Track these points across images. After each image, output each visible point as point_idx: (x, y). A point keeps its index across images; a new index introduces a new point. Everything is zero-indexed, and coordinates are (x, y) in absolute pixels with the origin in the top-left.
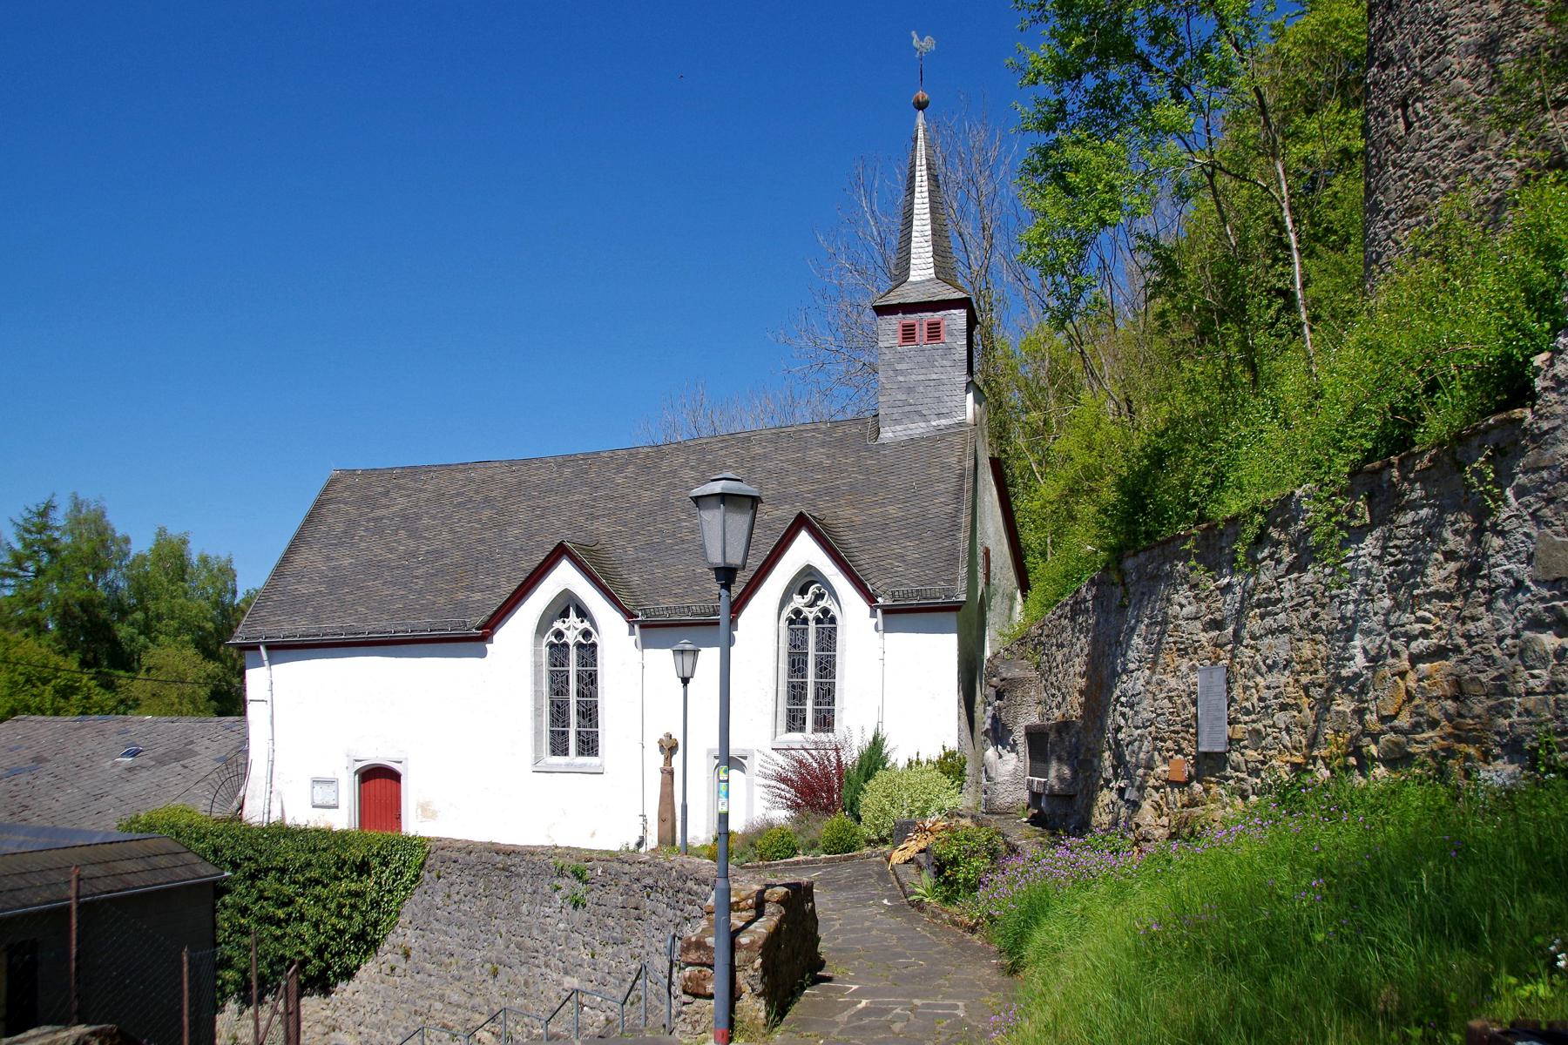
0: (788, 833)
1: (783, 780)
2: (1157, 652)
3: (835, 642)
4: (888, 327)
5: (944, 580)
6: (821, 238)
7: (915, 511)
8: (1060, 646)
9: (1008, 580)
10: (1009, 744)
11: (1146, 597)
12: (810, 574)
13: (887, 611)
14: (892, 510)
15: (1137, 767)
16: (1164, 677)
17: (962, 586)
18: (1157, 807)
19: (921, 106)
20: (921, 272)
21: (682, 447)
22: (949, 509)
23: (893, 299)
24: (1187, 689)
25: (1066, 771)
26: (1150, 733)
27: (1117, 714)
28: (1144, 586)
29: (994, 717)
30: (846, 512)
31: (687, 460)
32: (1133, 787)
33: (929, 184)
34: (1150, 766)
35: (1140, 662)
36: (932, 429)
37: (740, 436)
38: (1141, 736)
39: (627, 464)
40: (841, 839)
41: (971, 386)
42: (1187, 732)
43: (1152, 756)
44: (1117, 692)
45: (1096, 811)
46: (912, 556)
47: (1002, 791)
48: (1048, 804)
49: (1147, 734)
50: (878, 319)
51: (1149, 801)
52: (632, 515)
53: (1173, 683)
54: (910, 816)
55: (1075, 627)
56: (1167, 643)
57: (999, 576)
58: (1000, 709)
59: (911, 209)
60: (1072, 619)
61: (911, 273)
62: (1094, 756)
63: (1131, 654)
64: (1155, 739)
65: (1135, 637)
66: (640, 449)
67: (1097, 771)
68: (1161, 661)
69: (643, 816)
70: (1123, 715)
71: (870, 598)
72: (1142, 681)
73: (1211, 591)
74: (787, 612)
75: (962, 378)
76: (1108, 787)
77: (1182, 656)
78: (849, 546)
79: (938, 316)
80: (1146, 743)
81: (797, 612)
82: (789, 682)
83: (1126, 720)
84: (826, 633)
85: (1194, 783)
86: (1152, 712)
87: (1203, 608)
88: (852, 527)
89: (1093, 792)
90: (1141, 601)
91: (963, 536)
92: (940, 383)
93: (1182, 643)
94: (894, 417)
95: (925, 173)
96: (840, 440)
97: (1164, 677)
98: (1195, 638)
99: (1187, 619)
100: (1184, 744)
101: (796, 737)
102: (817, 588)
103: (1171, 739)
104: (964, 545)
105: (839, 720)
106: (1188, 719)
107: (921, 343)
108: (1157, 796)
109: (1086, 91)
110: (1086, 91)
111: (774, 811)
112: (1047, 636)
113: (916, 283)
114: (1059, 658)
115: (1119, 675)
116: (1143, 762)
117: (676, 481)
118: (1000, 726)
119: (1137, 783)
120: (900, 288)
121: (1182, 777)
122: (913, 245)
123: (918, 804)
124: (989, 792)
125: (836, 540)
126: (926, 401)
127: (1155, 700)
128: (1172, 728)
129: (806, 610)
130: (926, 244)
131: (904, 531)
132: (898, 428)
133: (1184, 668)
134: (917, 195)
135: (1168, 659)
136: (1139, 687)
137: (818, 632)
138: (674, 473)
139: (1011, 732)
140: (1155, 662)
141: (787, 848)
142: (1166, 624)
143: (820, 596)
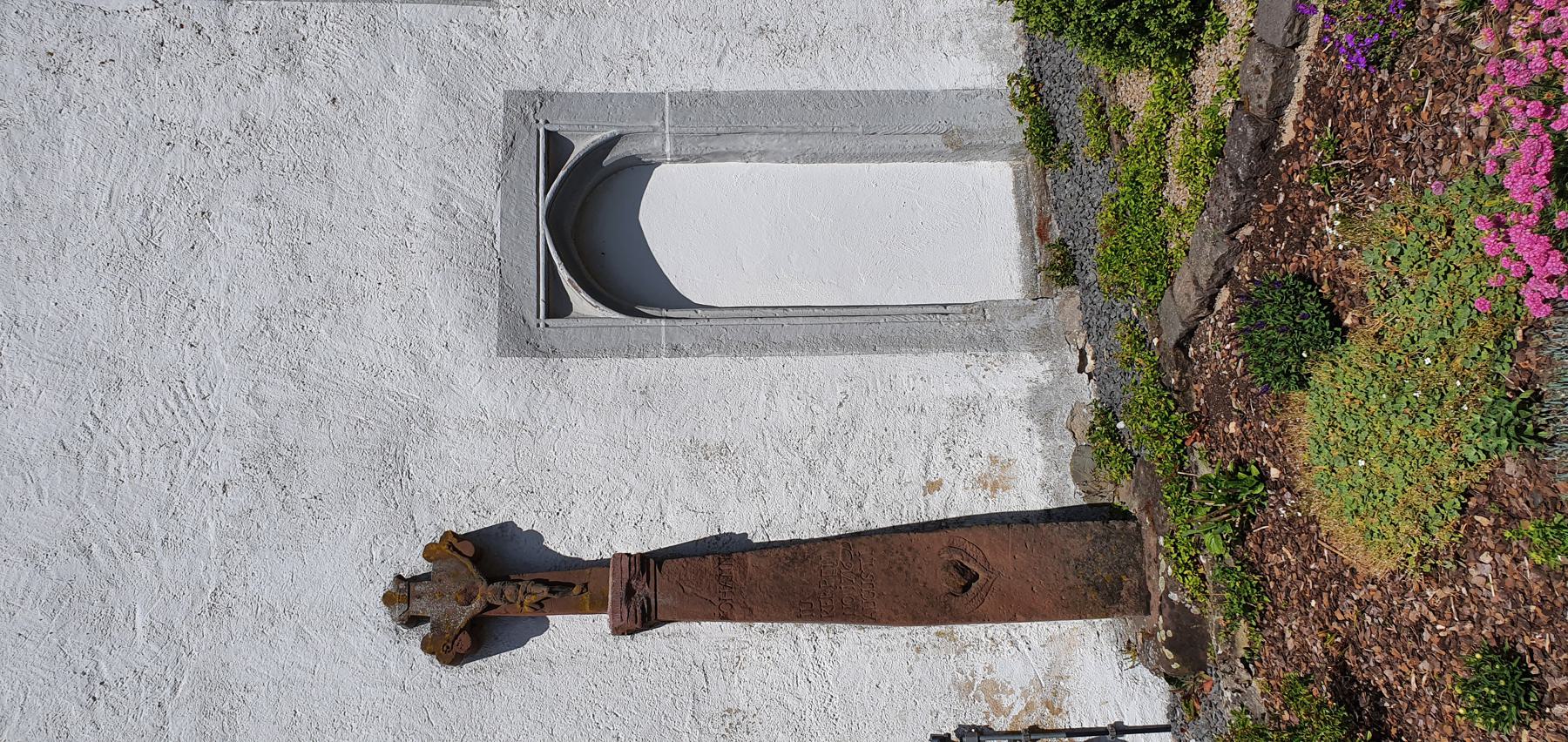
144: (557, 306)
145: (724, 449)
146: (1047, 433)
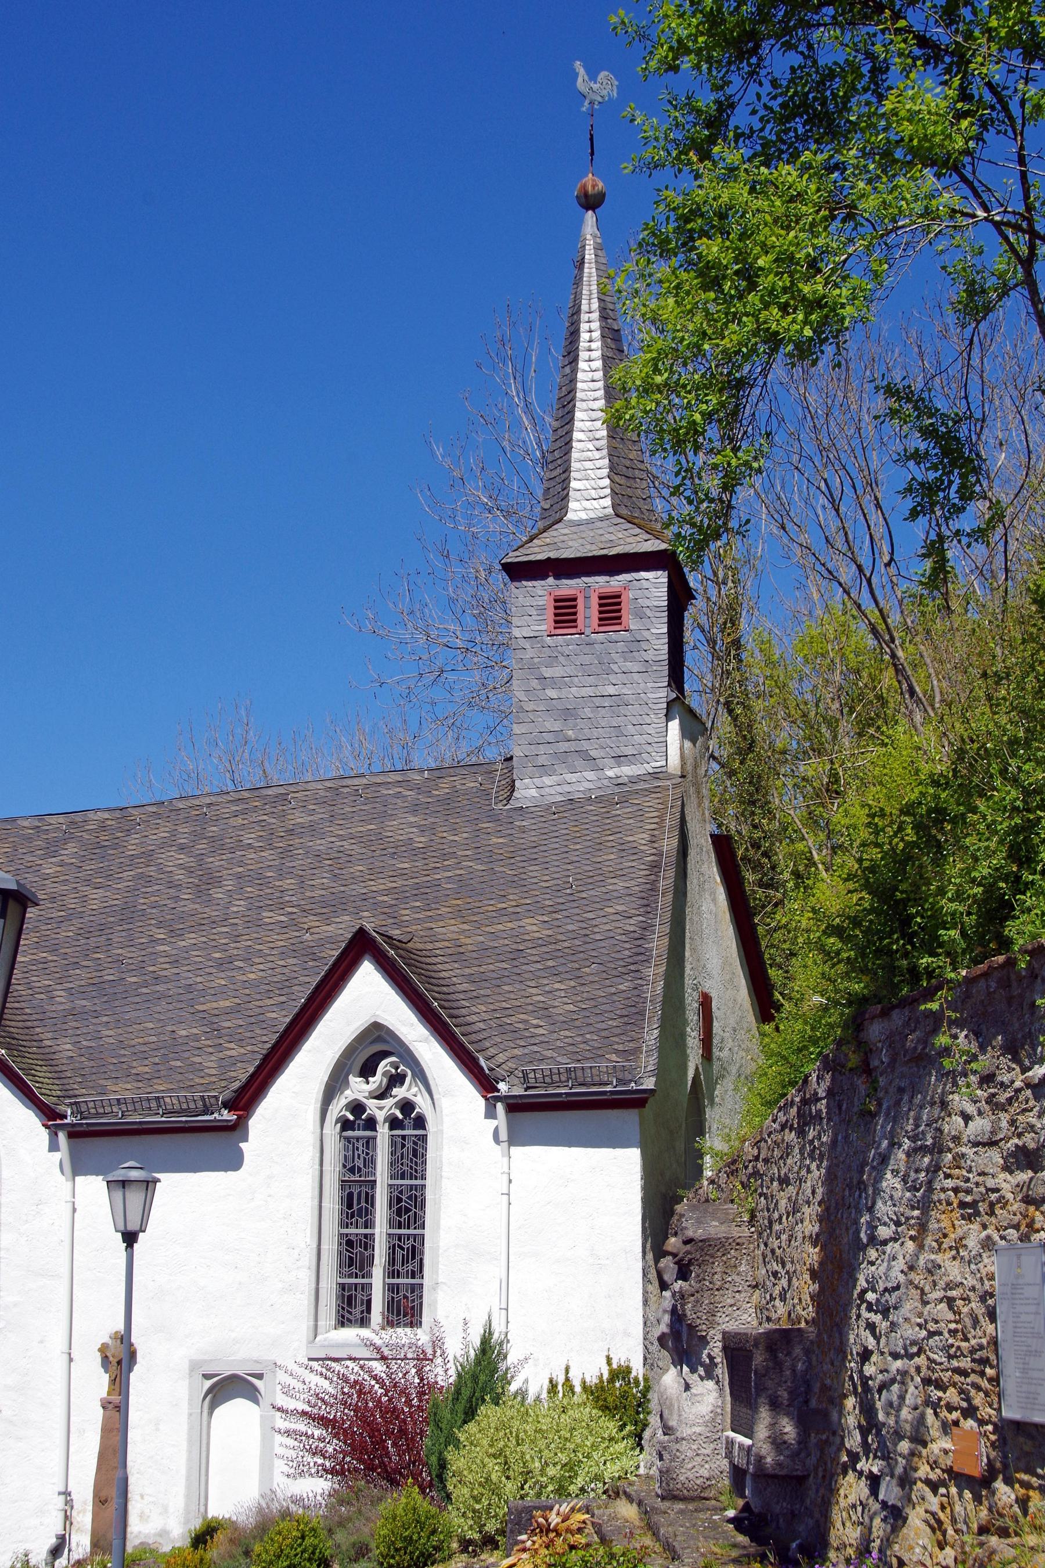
0: (313, 1529)
1: (323, 1421)
2: (925, 1205)
3: (424, 1163)
4: (529, 601)
5: (617, 1052)
6: (439, 452)
7: (570, 927)
8: (784, 1181)
9: (747, 1051)
10: (702, 1364)
11: (906, 1098)
12: (379, 1039)
13: (515, 1107)
14: (531, 926)
15: (898, 1436)
16: (938, 1258)
17: (648, 1062)
18: (936, 1526)
19: (591, 202)
20: (587, 504)
21: (164, 810)
22: (631, 925)
23: (538, 552)
24: (978, 1286)
25: (789, 1428)
26: (918, 1369)
27: (862, 1323)
28: (903, 1076)
29: (674, 1311)
30: (449, 929)
31: (173, 833)
32: (892, 1477)
33: (605, 346)
34: (920, 1440)
35: (898, 1224)
36: (606, 782)
37: (269, 792)
38: (904, 1373)
39: (66, 841)
40: (409, 1540)
41: (676, 708)
42: (982, 1374)
43: (922, 1417)
44: (862, 1283)
45: (837, 1516)
46: (563, 1007)
47: (690, 1454)
48: (755, 1491)
49: (912, 1371)
50: (512, 586)
51: (920, 1510)
52: (67, 932)
53: (954, 1271)
54: (539, 1495)
55: (804, 1146)
56: (943, 1190)
57: (729, 1044)
58: (682, 1297)
59: (572, 391)
60: (801, 1133)
61: (572, 505)
62: (831, 1401)
63: (883, 1208)
64: (927, 1382)
65: (889, 1175)
66: (91, 815)
67: (837, 1432)
68: (933, 1225)
69: (66, 1493)
70: (871, 1327)
71: (485, 1083)
72: (900, 1264)
73: (1018, 1091)
74: (338, 1107)
75: (660, 693)
76: (855, 1470)
77: (968, 1218)
78: (451, 990)
79: (615, 582)
80: (911, 1389)
81: (357, 1108)
82: (341, 1235)
83: (877, 1339)
84: (409, 1145)
85: (999, 1485)
86: (920, 1325)
87: (1004, 1124)
88: (458, 955)
89: (832, 1475)
90: (898, 1103)
91: (655, 972)
92: (619, 701)
93: (968, 1192)
94: (541, 761)
95: (596, 325)
96: (446, 801)
97: (938, 1258)
98: (990, 1183)
99: (976, 1144)
100: (978, 1399)
101: (350, 1334)
102: (392, 1064)
103: (954, 1385)
104: (655, 989)
105: (429, 1305)
106: (981, 1347)
107: (588, 631)
108: (934, 1502)
109: (774, 83)
110: (774, 83)
111: (301, 1481)
112: (766, 1161)
113: (579, 523)
114: (783, 1203)
115: (864, 1248)
116: (908, 1427)
117: (152, 871)
118: (685, 1329)
119: (899, 1470)
120: (551, 533)
121: (976, 1469)
122: (575, 455)
123: (551, 1471)
124: (666, 1456)
125: (428, 979)
126: (595, 733)
127: (925, 1303)
128: (955, 1363)
129: (372, 1104)
130: (597, 455)
131: (550, 963)
132: (547, 781)
133: (972, 1243)
134: (582, 365)
135: (945, 1224)
136: (897, 1275)
137: (393, 1143)
138: (148, 856)
139: (704, 1341)
140: (923, 1227)
141: (310, 1560)
142: (941, 1152)
143: (396, 1079)
144: (206, 1377)
145: (157, 1429)
146: (155, 1535)
